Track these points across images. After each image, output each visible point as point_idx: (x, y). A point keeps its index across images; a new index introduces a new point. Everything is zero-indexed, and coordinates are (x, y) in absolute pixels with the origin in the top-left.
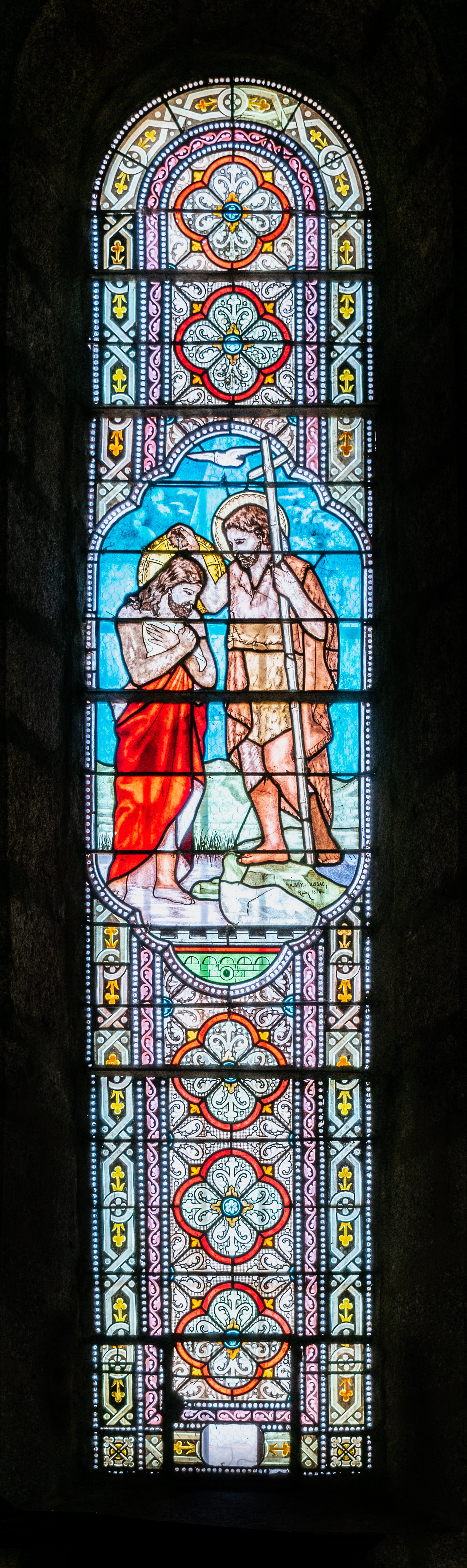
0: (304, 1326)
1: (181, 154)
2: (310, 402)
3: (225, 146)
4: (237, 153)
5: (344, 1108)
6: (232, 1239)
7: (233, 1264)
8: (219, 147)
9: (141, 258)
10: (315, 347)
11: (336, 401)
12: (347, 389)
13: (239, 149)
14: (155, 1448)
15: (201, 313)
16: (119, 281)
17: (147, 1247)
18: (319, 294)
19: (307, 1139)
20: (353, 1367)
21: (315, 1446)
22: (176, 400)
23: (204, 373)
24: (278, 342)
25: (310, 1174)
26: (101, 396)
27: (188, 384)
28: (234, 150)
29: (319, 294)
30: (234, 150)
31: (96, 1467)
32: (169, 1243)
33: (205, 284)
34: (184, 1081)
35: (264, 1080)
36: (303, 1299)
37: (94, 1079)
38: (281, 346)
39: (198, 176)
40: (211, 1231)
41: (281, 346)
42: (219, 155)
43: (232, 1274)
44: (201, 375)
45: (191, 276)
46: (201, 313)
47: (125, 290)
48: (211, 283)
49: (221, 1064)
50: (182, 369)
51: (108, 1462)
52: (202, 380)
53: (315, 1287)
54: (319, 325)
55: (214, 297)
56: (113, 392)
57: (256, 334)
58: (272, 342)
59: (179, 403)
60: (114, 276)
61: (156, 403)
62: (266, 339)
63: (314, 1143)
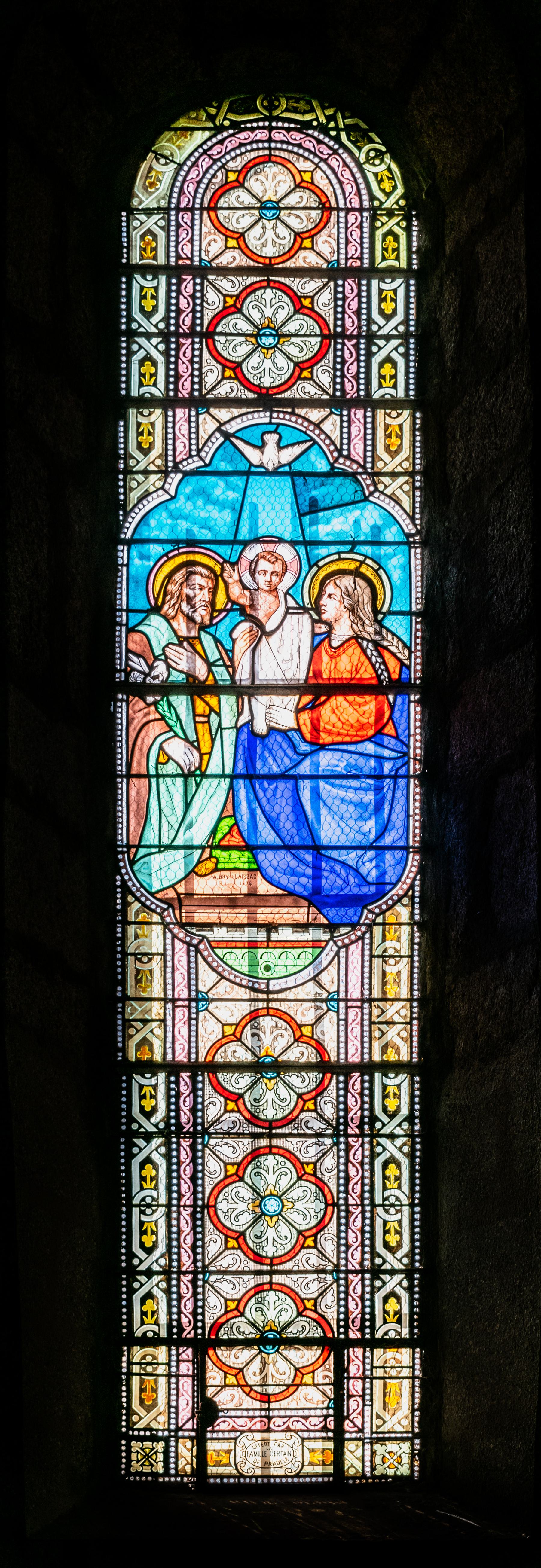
0: (346, 1259)
1: (215, 153)
2: (348, 396)
3: (261, 145)
4: (273, 152)
5: (392, 1305)
6: (270, 1102)
7: (270, 1147)
8: (255, 146)
9: (172, 1454)
10: (354, 342)
11: (376, 396)
12: (388, 383)
13: (276, 149)
14: (186, 1452)
15: (233, 307)
16: (149, 274)
17: (179, 1178)
18: (358, 355)
19: (352, 1272)
20: (400, 1372)
21: (359, 1453)
22: (208, 393)
23: (237, 367)
24: (316, 336)
25: (354, 1104)
26: (128, 389)
27: (223, 1247)
28: (270, 149)
29: (358, 355)
30: (270, 149)
31: (124, 1265)
32: (204, 1243)
33: (240, 278)
34: (219, 1352)
35: (304, 1074)
36: (346, 1232)
37: (119, 960)
38: (319, 339)
39: (232, 177)
40: (245, 363)
41: (319, 339)
42: (254, 154)
43: (271, 1273)
44: (235, 370)
45: (224, 271)
46: (233, 307)
47: (155, 283)
48: (245, 278)
49: (259, 1058)
50: (216, 1095)
51: (136, 1467)
52: (235, 373)
53: (359, 1219)
54: (358, 384)
55: (250, 290)
56: (141, 385)
57: (292, 327)
58: (310, 336)
59: (210, 396)
60: (144, 270)
61: (187, 396)
62: (302, 332)
63: (358, 1267)
